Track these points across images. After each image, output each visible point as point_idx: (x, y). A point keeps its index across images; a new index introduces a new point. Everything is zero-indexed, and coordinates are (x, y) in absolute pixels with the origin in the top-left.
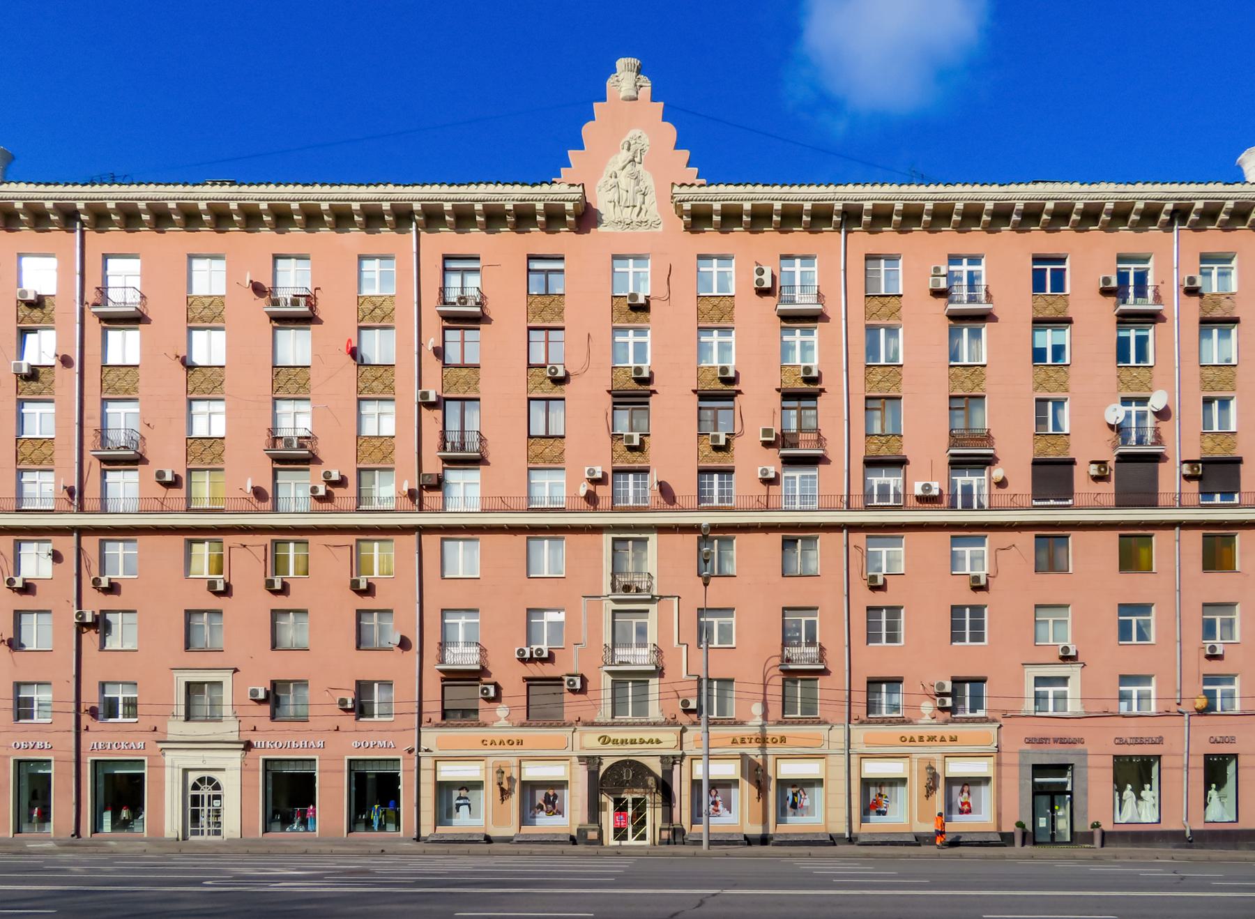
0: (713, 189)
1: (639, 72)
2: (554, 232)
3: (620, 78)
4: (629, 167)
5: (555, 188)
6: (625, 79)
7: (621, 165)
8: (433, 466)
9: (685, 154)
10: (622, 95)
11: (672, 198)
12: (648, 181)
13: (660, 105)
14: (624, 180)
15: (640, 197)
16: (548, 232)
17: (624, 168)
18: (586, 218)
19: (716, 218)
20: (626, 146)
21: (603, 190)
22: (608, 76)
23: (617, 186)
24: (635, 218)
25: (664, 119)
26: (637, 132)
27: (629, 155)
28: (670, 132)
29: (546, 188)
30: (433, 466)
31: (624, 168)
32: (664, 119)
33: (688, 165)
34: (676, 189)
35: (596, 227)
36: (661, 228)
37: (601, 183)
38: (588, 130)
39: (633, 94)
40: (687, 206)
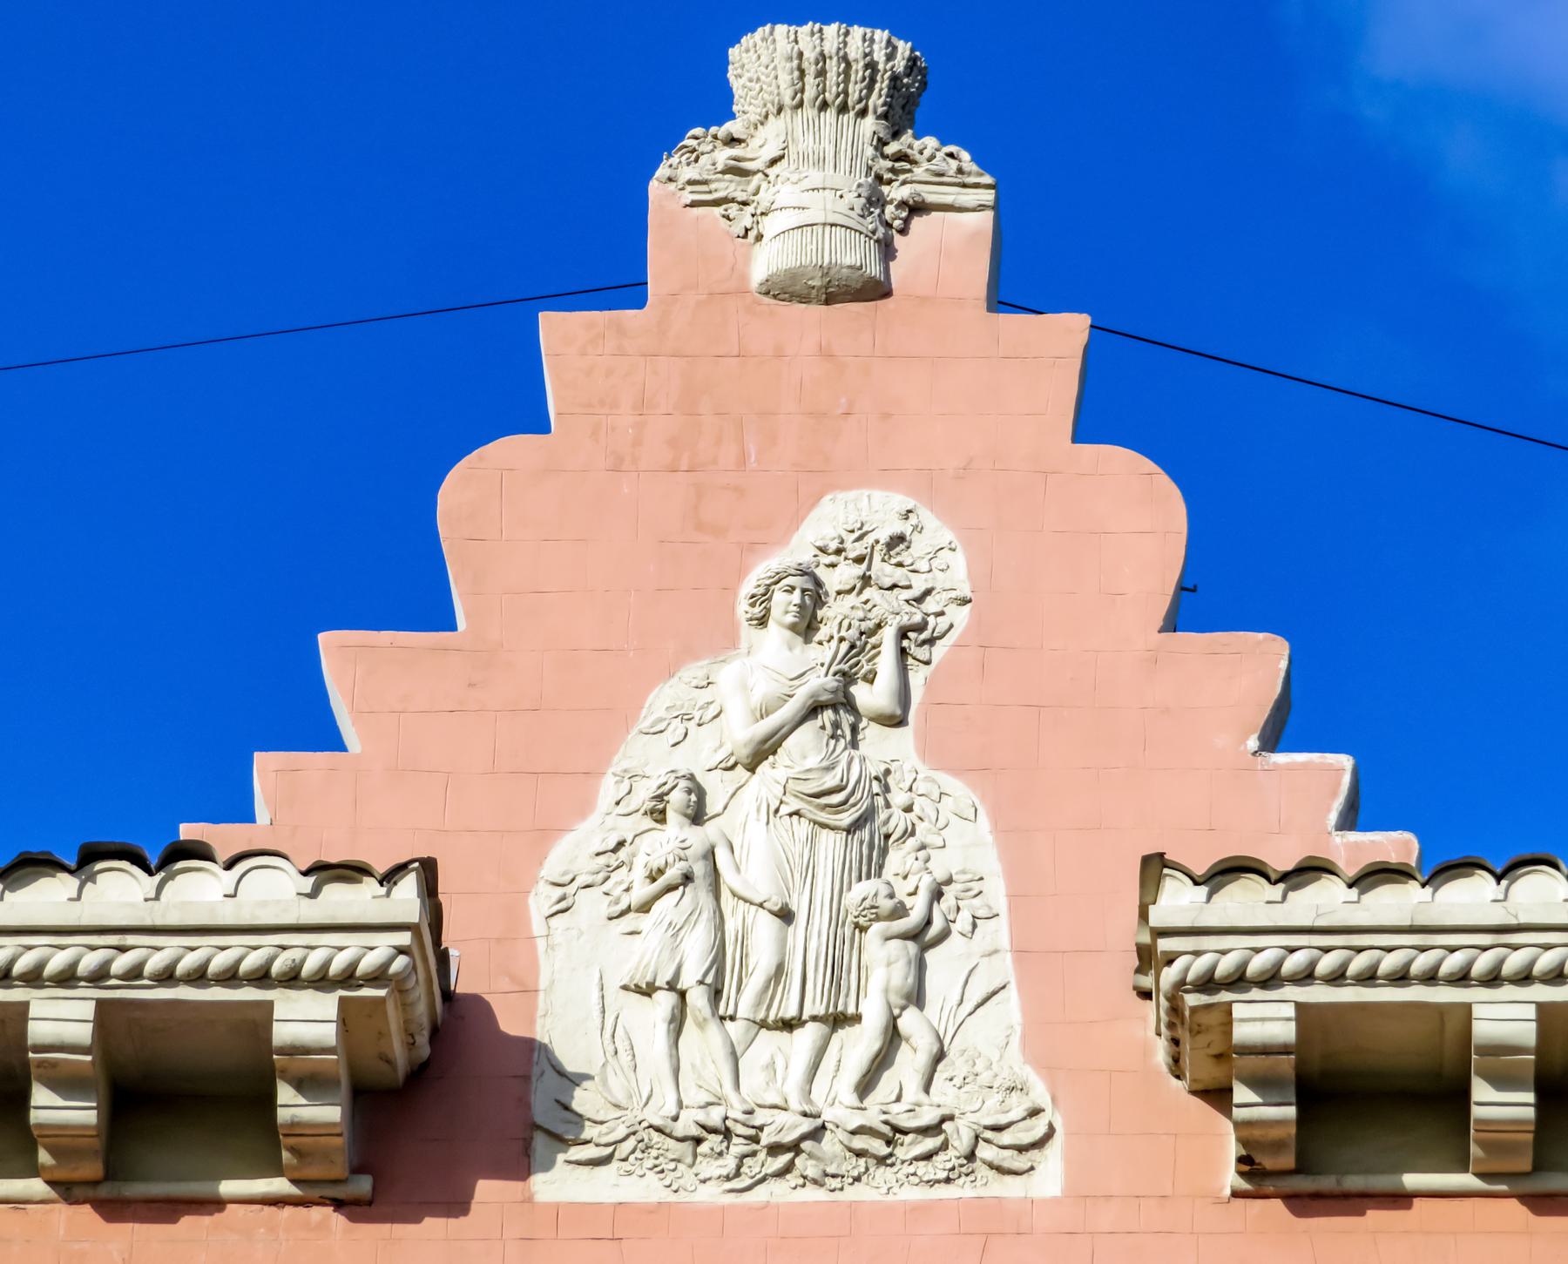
0: (1471, 897)
1: (902, 112)
2: (169, 1209)
3: (760, 148)
4: (806, 748)
5: (198, 892)
6: (783, 161)
7: (742, 732)
8: (661, 982)
9: (1257, 663)
10: (765, 263)
11: (1147, 958)
12: (956, 835)
13: (1066, 334)
14: (759, 840)
15: (883, 962)
16: (114, 1210)
17: (764, 751)
18: (442, 1093)
19: (1500, 1104)
20: (784, 605)
21: (591, 906)
22: (669, 141)
23: (704, 876)
24: (836, 1099)
25: (1090, 425)
26: (882, 510)
27: (813, 668)
28: (1139, 515)
29: (120, 892)
30: (661, 982)
31: (764, 751)
32: (1090, 425)
33: (1273, 738)
34: (1179, 901)
35: (520, 1166)
36: (1049, 1176)
37: (574, 851)
38: (484, 500)
39: (854, 254)
40: (1265, 1020)
